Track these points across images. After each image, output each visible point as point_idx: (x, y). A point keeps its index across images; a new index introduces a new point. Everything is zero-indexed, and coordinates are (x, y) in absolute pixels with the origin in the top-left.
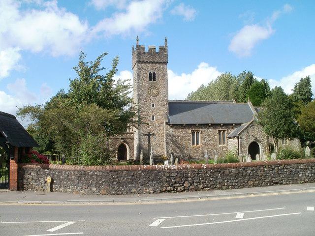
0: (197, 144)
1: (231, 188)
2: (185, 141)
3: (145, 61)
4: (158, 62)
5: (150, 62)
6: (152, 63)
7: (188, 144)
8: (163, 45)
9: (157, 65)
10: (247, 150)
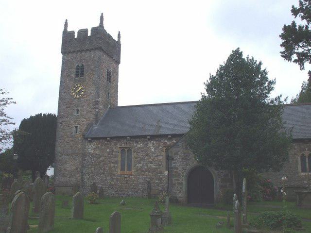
0: (129, 169)
1: (295, 61)
2: (109, 165)
3: (72, 50)
4: (87, 50)
5: (78, 51)
6: (81, 51)
7: (113, 169)
8: (97, 24)
9: (88, 54)
10: (184, 183)
